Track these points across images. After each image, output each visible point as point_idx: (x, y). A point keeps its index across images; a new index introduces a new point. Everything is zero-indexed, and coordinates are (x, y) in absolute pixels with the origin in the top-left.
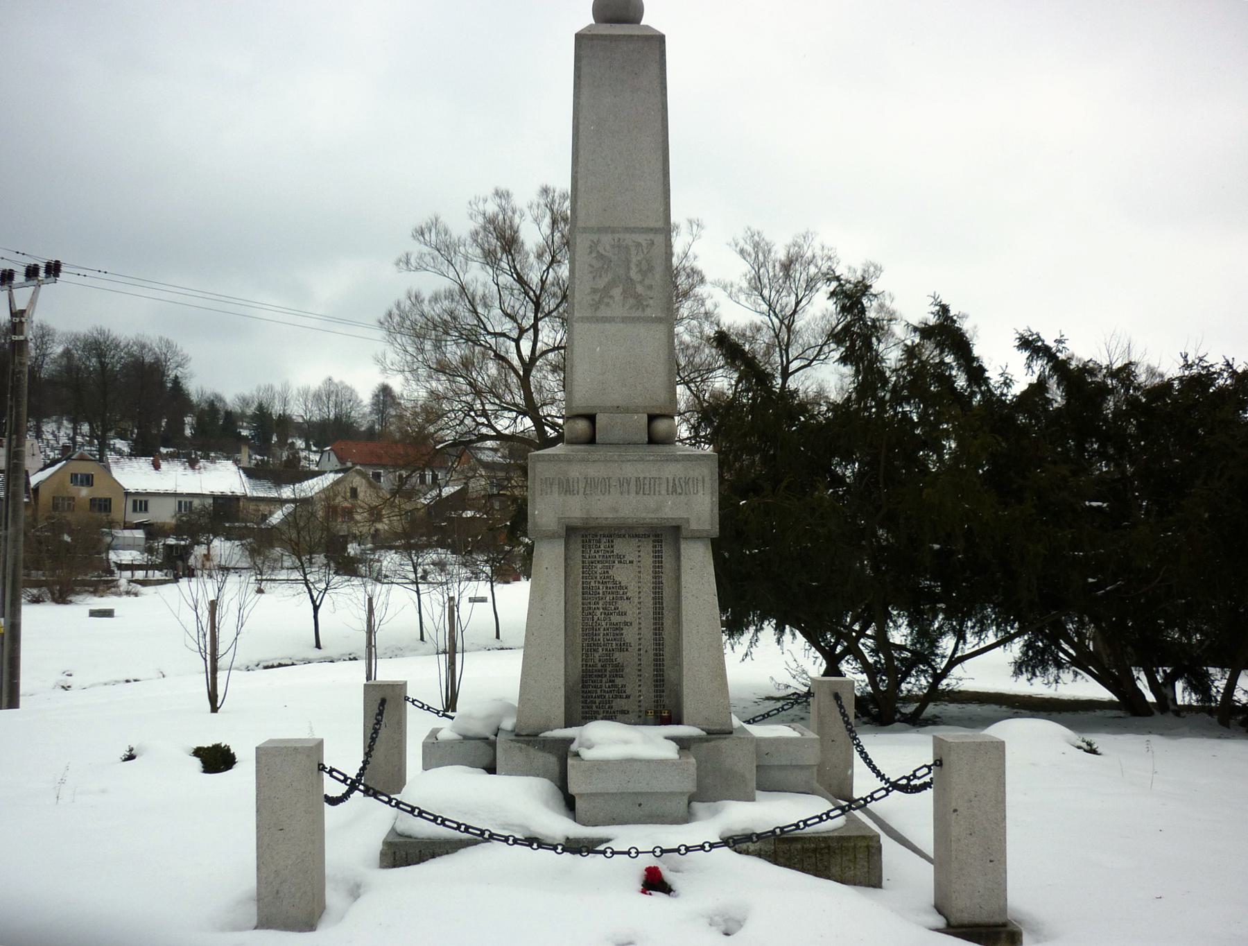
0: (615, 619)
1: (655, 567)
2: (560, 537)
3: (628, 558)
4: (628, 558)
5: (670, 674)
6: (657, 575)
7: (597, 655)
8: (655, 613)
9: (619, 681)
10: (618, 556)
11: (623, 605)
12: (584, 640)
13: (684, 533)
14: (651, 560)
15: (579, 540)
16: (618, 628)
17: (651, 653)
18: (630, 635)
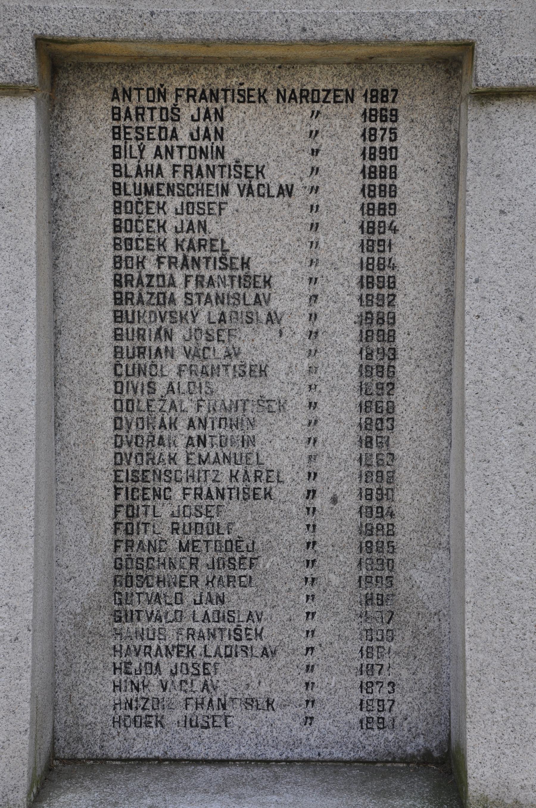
0: (229, 389)
1: (367, 209)
2: (31, 91)
3: (274, 177)
4: (274, 177)
5: (418, 578)
6: (377, 281)
7: (165, 510)
8: (365, 371)
9: (239, 600)
10: (241, 169)
11: (254, 342)
12: (119, 459)
13: (487, 72)
14: (355, 182)
15: (103, 106)
16: (234, 416)
17: (350, 503)
18: (279, 445)
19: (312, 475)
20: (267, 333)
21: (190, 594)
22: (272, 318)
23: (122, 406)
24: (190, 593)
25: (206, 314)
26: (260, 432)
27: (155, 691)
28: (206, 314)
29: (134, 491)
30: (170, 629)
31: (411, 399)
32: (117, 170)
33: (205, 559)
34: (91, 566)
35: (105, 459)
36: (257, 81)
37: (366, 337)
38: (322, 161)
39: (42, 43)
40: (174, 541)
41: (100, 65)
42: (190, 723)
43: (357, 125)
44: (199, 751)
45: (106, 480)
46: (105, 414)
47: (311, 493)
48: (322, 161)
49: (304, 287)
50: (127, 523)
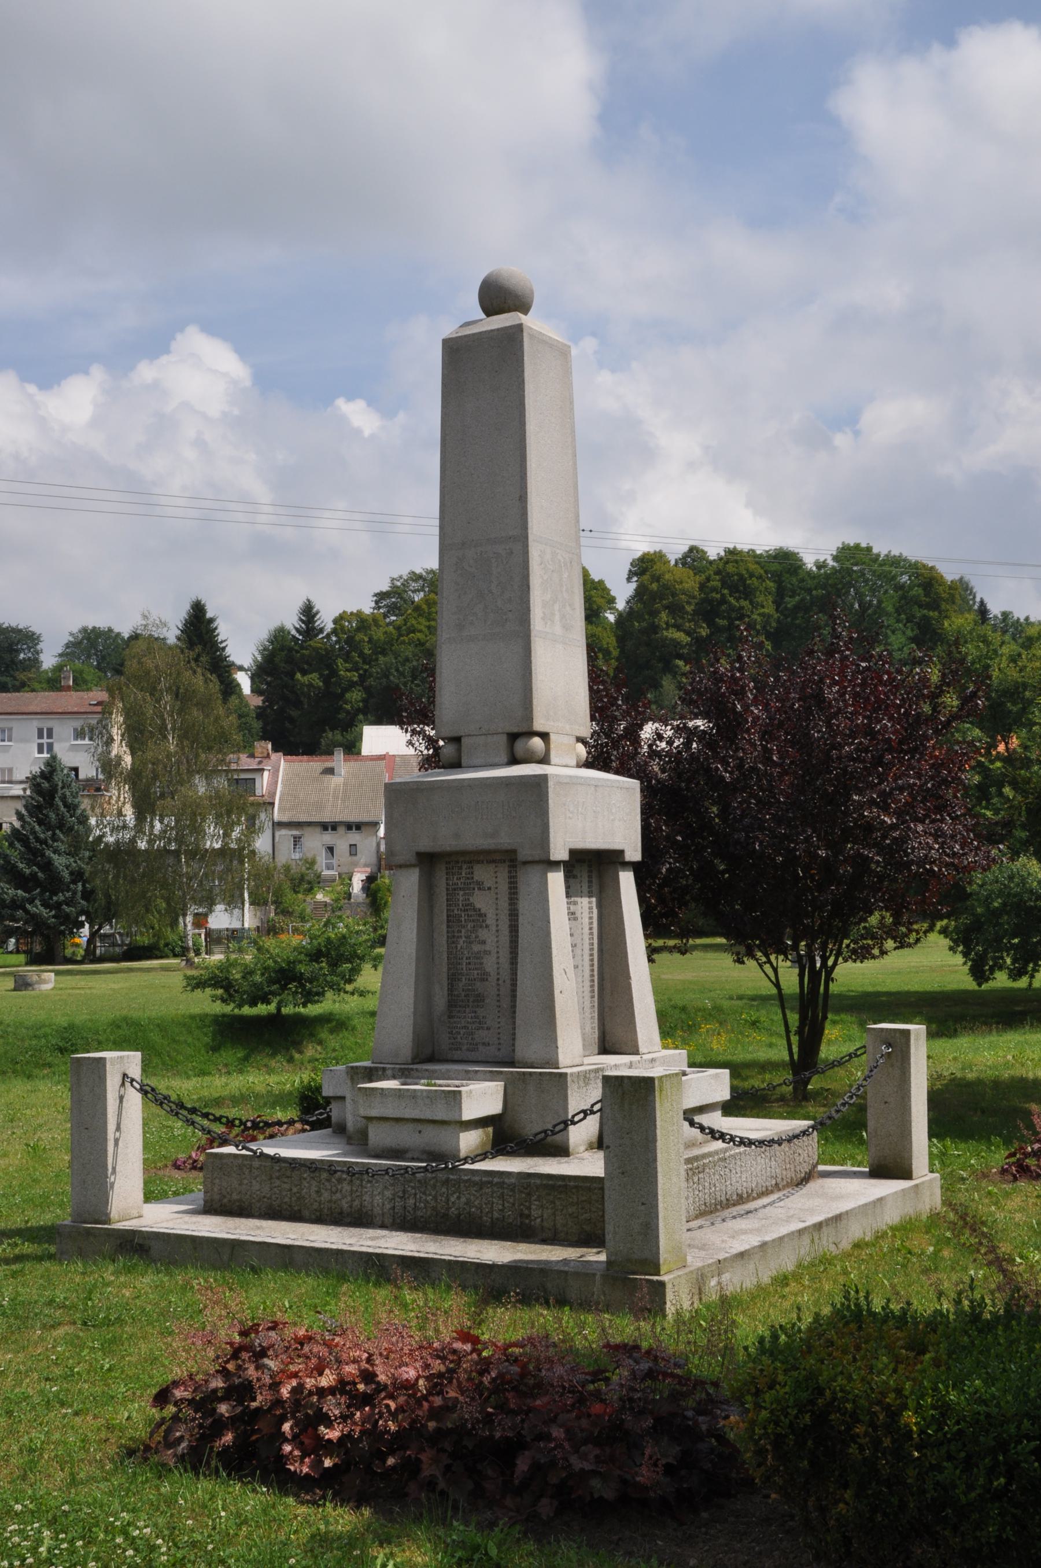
0: (476, 948)
1: (510, 893)
3: (487, 885)
4: (487, 885)
7: (461, 985)
11: (483, 934)
12: (449, 969)
14: (507, 886)
18: (489, 964)
19: (498, 974)
20: (485, 931)
21: (468, 1010)
22: (487, 926)
23: (449, 953)
24: (468, 1010)
25: (470, 925)
26: (485, 961)
27: (459, 1040)
28: (470, 925)
29: (453, 978)
30: (463, 1021)
31: (25, 717)
32: (448, 884)
33: (471, 1000)
34: (440, 1000)
35: (445, 970)
36: (481, 858)
37: (511, 932)
38: (499, 880)
39: (198, 610)
40: (463, 994)
41: (756, 1210)
42: (468, 1050)
43: (507, 870)
44: (471, 1058)
45: (445, 975)
46: (445, 956)
47: (498, 979)
50: (451, 989)
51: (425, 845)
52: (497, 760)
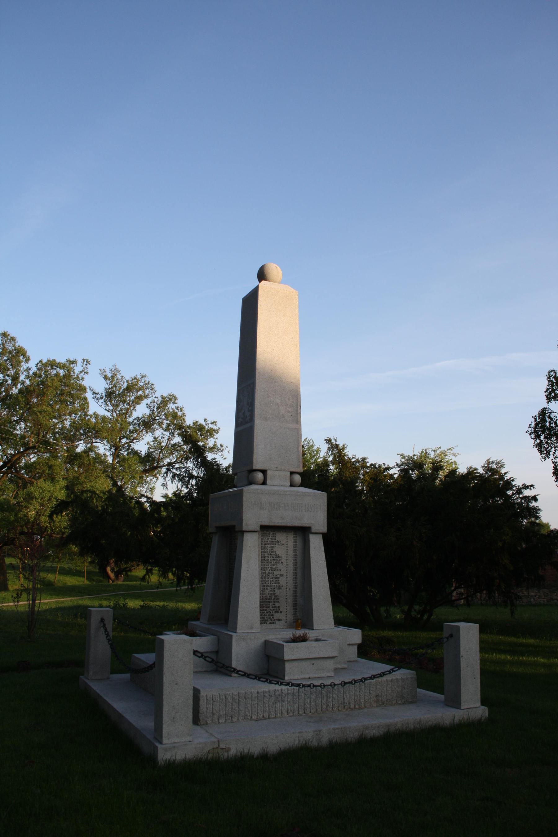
0: (276, 573)
9: (277, 604)
10: (278, 541)
11: (280, 566)
13: (313, 530)
18: (282, 581)
20: (281, 565)
24: (271, 604)
32: (262, 541)
38: (286, 608)
40: (268, 596)
48: (286, 608)
49: (286, 558)
51: (266, 522)
52: (285, 483)
